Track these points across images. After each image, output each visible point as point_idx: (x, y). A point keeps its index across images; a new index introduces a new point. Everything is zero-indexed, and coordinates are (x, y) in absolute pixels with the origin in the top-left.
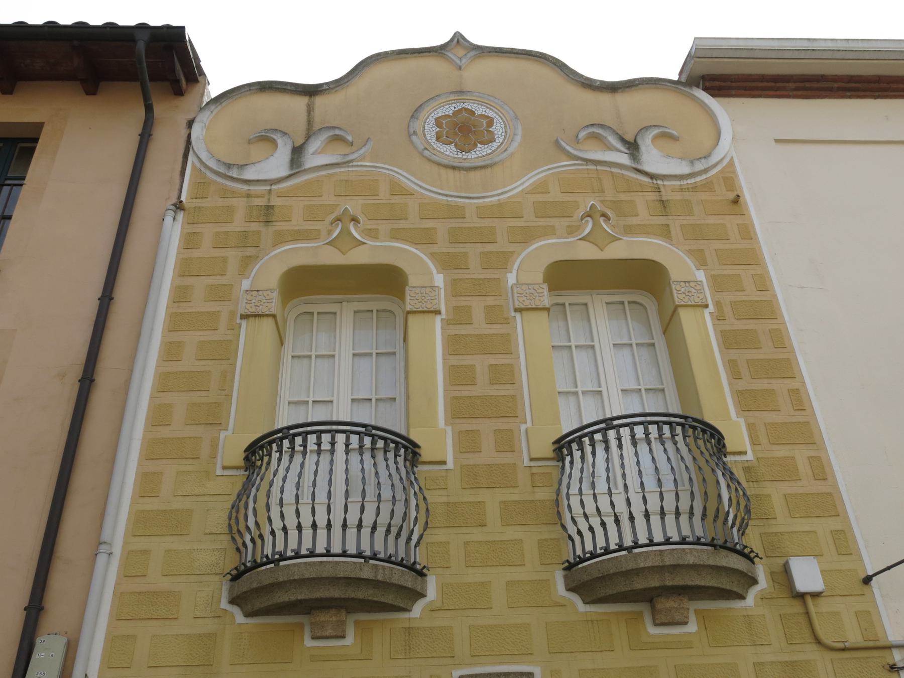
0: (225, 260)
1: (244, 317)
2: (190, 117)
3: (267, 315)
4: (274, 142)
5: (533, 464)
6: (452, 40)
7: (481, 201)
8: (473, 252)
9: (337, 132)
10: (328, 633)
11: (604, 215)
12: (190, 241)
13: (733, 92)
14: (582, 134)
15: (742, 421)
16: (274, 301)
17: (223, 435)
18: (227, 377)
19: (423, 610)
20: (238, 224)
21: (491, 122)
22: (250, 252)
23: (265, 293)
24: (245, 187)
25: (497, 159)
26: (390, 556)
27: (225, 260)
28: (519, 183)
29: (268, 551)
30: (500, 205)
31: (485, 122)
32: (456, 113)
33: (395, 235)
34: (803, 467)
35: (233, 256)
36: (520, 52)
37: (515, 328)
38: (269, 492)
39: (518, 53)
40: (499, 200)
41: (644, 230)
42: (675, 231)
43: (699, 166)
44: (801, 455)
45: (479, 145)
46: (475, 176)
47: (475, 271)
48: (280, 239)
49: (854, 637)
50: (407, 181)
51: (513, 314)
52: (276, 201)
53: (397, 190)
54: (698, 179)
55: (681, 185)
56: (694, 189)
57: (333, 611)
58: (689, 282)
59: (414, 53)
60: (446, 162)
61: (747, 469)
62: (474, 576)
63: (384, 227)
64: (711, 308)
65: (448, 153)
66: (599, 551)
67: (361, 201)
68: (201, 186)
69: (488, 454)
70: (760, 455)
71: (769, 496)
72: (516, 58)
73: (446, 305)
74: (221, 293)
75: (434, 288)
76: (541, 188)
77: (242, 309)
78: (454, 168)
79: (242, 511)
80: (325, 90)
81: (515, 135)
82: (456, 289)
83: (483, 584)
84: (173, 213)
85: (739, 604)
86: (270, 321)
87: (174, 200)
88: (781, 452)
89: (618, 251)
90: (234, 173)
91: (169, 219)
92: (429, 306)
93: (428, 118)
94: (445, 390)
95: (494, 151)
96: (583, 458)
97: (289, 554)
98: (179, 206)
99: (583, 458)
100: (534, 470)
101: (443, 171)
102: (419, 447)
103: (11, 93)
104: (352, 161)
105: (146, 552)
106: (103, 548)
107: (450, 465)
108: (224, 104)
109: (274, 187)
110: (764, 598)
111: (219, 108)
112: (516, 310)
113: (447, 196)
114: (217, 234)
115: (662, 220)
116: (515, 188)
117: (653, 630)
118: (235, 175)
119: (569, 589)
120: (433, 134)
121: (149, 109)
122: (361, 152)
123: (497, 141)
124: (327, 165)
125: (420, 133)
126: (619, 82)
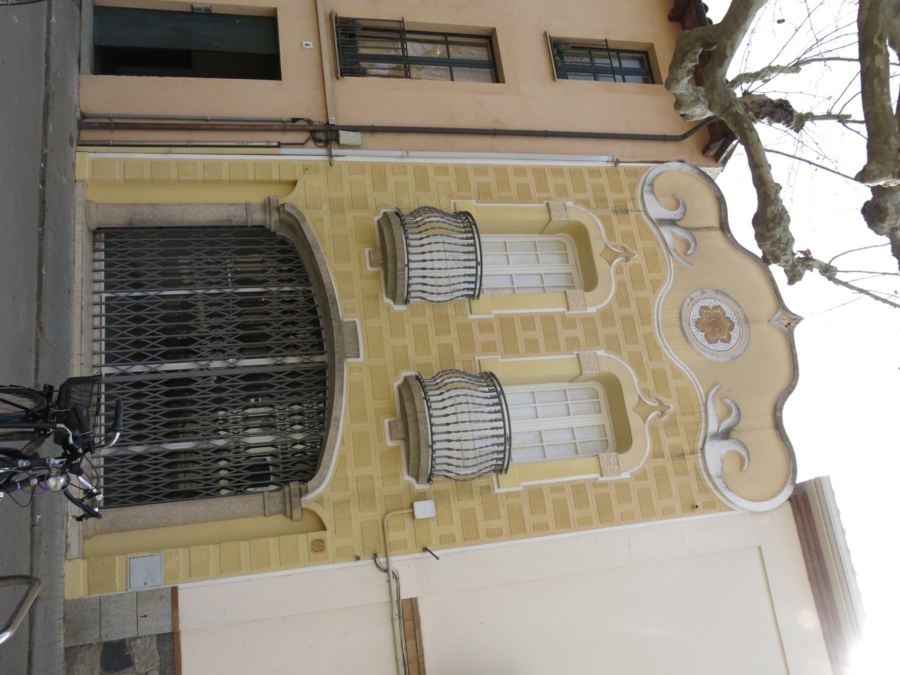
0: (585, 191)
1: (548, 205)
2: (686, 160)
3: (550, 216)
4: (677, 208)
5: (477, 362)
6: (793, 314)
7: (658, 335)
8: (618, 330)
9: (693, 245)
10: (371, 256)
11: (663, 413)
12: (595, 172)
13: (799, 518)
14: (728, 401)
15: (521, 488)
16: (561, 219)
17: (474, 201)
18: (509, 200)
19: (387, 304)
20: (611, 196)
21: (728, 341)
22: (593, 204)
23: (565, 214)
24: (639, 197)
25: (693, 344)
26: (434, 468)
27: (585, 191)
28: (677, 358)
29: (430, 393)
30: (657, 347)
31: (725, 337)
32: (728, 319)
33: (621, 285)
34: (494, 524)
35: (589, 195)
36: (795, 361)
37: (565, 354)
38: (465, 388)
39: (793, 360)
40: (661, 347)
41: (656, 440)
42: (660, 462)
43: (718, 482)
44: (502, 523)
45: (703, 334)
46: (678, 330)
47: (603, 332)
48: (605, 220)
49: (392, 536)
50: (664, 289)
51: (575, 353)
52: (632, 215)
53: (656, 285)
54: (709, 483)
55: (700, 470)
56: (699, 479)
57: (382, 257)
58: (618, 464)
59: (775, 290)
60: (684, 311)
61: (489, 488)
62: (409, 329)
63: (626, 277)
64: (601, 479)
65: (692, 313)
66: (408, 241)
67: (643, 263)
68: (635, 173)
69: (479, 338)
70: (499, 497)
71: (473, 499)
72: (790, 360)
73: (576, 314)
74: (562, 191)
75: (585, 306)
76: (677, 374)
77: (553, 205)
78: (680, 317)
79: (454, 375)
80: (727, 236)
81: (717, 356)
82: (588, 320)
83: (404, 333)
84: (611, 160)
85: (405, 471)
86: (577, 372)
87: (621, 159)
88: (503, 511)
89: (634, 420)
90: (646, 188)
91: (606, 158)
92: (571, 303)
93: (719, 300)
94: (517, 314)
95: (701, 344)
96: (488, 405)
97: (431, 412)
98: (617, 162)
99: (488, 405)
100: (473, 362)
101: (677, 311)
102: (506, 473)
103: (670, 20)
104: (671, 255)
105: (406, 173)
106: (405, 153)
107: (470, 317)
108: (700, 178)
109: (643, 213)
110: (410, 487)
111: (697, 176)
112: (578, 355)
113: (657, 314)
114: (602, 185)
115: (667, 452)
116: (673, 357)
117: (386, 421)
118: (644, 189)
119: (405, 378)
120: (707, 304)
121: (684, 136)
122: (680, 260)
123: (710, 345)
124: (665, 240)
125: (705, 296)
126: (784, 430)
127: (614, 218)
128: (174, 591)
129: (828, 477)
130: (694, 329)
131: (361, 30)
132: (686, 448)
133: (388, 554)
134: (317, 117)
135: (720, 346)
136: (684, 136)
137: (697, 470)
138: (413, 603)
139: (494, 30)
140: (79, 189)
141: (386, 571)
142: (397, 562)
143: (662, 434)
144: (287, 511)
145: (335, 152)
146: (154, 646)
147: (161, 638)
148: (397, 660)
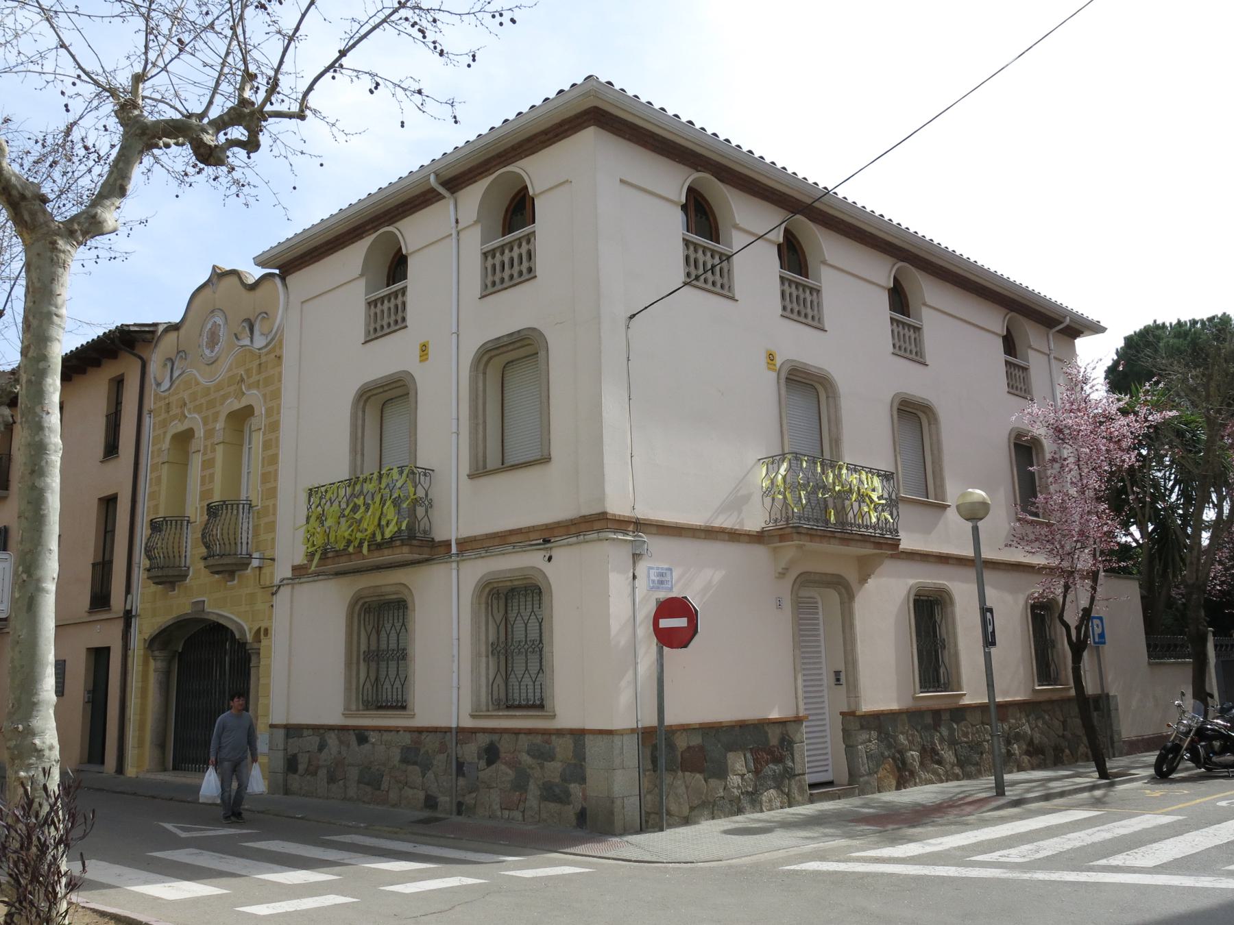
49: (268, 583)
73: (36, 500)
129: (254, 259)
136: (141, 358)
139: (100, 499)
140: (141, 776)
141: (279, 586)
142: (277, 581)
145: (134, 613)
147: (287, 736)
148: (314, 581)
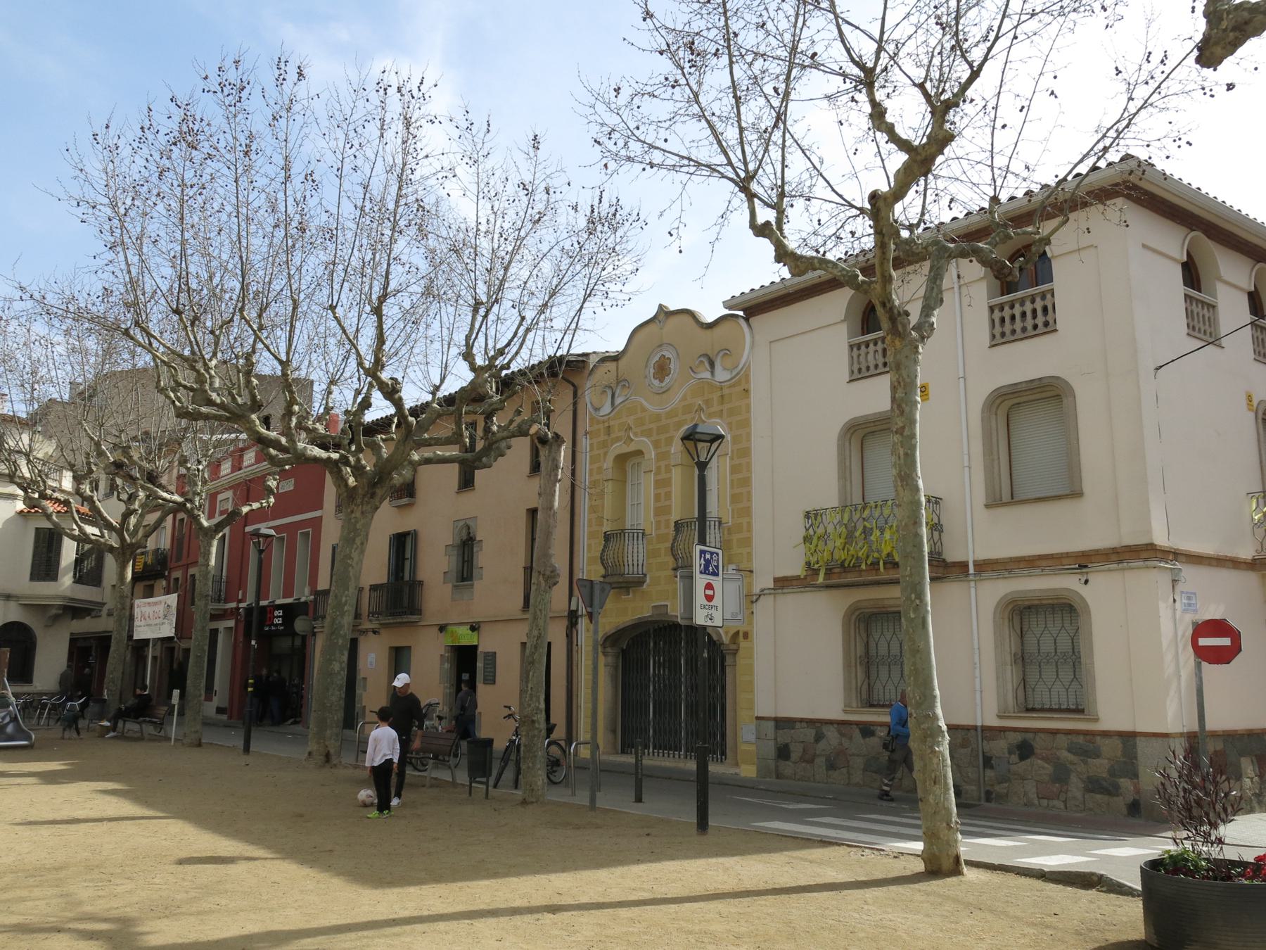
35: (601, 452)
42: (725, 413)
43: (734, 373)
52: (612, 423)
53: (644, 410)
67: (632, 417)
76: (684, 398)
121: (573, 385)
127: (613, 436)
128: (758, 718)
130: (663, 385)
131: (93, 610)
132: (719, 393)
133: (835, 592)
134: (565, 623)
135: (672, 366)
136: (573, 385)
137: (730, 387)
138: (776, 580)
142: (756, 590)
143: (712, 410)
144: (735, 652)
146: (781, 731)
